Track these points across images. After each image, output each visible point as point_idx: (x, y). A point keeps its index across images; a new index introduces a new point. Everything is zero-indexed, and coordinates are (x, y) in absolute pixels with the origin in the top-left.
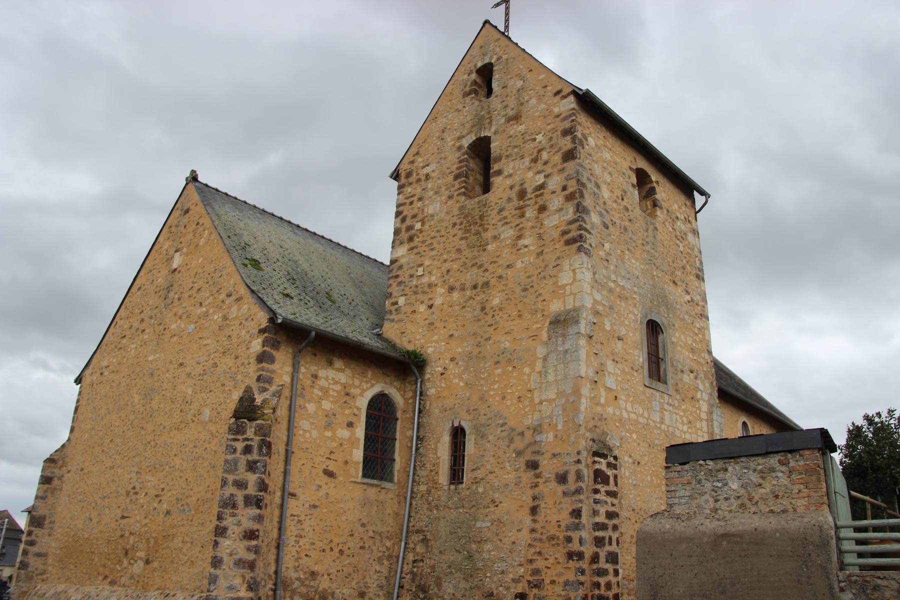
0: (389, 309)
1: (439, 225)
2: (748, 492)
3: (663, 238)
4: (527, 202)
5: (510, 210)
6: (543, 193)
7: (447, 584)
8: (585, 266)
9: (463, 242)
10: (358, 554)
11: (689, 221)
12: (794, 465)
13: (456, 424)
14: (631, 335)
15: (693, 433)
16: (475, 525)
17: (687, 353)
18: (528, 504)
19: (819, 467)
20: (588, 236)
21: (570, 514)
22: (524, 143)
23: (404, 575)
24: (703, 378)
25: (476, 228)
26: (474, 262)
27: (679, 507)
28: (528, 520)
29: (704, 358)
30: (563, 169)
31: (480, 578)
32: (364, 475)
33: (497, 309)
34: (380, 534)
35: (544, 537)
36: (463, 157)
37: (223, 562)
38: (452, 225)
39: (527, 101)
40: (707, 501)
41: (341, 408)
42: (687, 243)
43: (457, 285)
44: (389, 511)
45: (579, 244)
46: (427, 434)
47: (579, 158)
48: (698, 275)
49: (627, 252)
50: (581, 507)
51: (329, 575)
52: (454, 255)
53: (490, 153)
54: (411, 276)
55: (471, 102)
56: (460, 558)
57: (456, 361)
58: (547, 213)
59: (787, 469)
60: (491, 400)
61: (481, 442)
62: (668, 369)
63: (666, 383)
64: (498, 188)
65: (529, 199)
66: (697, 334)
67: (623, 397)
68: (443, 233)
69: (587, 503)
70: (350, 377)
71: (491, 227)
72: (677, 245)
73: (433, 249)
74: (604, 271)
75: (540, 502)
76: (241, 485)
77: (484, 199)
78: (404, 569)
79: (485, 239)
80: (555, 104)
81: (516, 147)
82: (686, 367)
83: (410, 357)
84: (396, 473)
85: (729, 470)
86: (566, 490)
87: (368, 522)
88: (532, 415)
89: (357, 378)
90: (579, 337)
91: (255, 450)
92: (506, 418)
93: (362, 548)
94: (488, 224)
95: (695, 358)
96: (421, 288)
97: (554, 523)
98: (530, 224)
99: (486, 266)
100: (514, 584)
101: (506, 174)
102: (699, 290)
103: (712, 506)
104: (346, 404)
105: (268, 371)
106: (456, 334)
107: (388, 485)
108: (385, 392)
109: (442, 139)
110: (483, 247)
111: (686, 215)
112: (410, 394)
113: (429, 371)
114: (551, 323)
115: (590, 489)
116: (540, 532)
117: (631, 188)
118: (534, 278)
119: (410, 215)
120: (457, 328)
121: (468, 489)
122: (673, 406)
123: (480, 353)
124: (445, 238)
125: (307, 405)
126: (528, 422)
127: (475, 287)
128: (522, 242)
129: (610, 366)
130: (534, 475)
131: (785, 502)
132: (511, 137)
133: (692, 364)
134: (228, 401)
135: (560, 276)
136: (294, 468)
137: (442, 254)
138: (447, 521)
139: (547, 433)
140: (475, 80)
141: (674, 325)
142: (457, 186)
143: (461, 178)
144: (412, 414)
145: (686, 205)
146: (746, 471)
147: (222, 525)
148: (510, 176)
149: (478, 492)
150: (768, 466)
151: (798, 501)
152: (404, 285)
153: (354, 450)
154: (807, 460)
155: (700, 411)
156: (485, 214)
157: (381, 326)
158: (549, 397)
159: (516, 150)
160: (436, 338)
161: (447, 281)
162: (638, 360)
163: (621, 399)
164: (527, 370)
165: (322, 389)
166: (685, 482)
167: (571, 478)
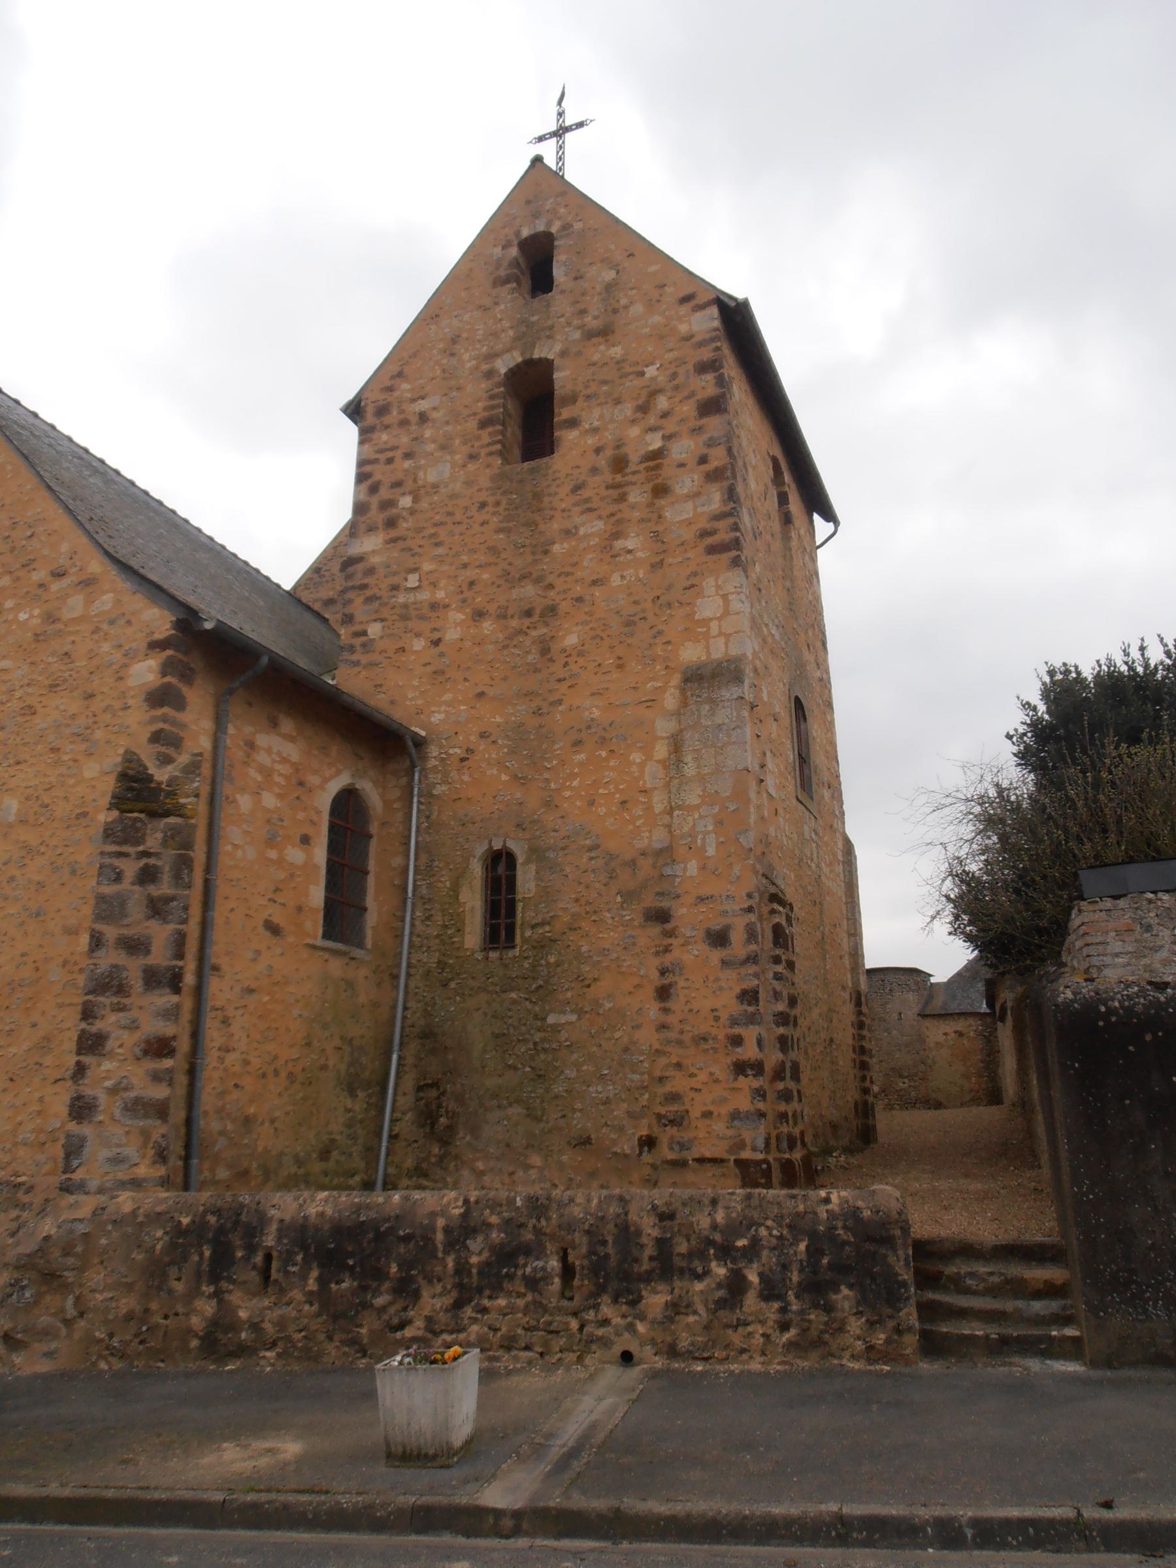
4: (630, 478)
5: (595, 487)
13: (497, 845)
22: (621, 377)
28: (653, 1011)
35: (687, 1038)
37: (96, 1106)
39: (626, 307)
43: (492, 608)
51: (272, 1121)
60: (565, 805)
65: (634, 473)
73: (437, 545)
75: (676, 978)
76: (135, 946)
78: (398, 1104)
81: (605, 382)
84: (369, 933)
88: (650, 832)
91: (166, 877)
96: (416, 609)
98: (637, 514)
101: (587, 426)
105: (174, 723)
106: (491, 692)
107: (358, 953)
112: (396, 793)
120: (492, 683)
125: (238, 796)
128: (619, 544)
134: (72, 782)
136: (219, 914)
137: (457, 555)
147: (94, 1029)
148: (595, 430)
160: (448, 697)
164: (636, 757)
165: (261, 769)
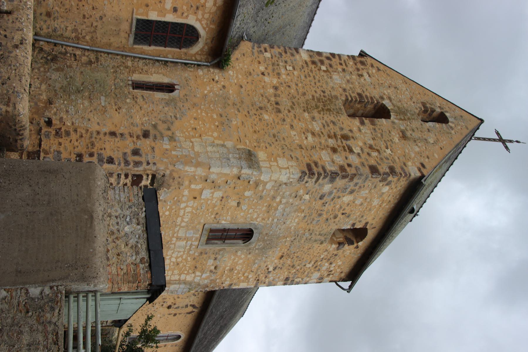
0: (262, 46)
1: (324, 81)
2: (122, 237)
3: (315, 248)
4: (339, 141)
6: (346, 151)
7: (58, 75)
8: (292, 176)
9: (311, 97)
10: (79, 13)
11: (329, 275)
12: (140, 267)
13: (176, 87)
14: (242, 214)
15: (170, 266)
16: (102, 95)
17: (229, 265)
18: (118, 130)
19: (139, 283)
20: (314, 180)
21: (110, 156)
23: (64, 47)
24: (212, 278)
25: (321, 106)
26: (296, 104)
27: (113, 194)
29: (225, 280)
30: (364, 165)
31: (63, 97)
32: (138, 20)
33: (261, 117)
34: (95, 32)
35: (93, 139)
36: (375, 100)
38: (324, 90)
39: (417, 145)
40: (116, 211)
41: (187, 3)
42: (312, 271)
43: (279, 92)
44: (112, 40)
45: (308, 172)
46: (169, 68)
47: (372, 177)
48: (288, 280)
49: (303, 215)
50: (115, 164)
52: (301, 91)
53: (378, 118)
54: (286, 62)
55: (417, 107)
56: (78, 84)
57: (223, 89)
58: (331, 153)
59: (138, 262)
61: (163, 103)
62: (217, 246)
63: (207, 244)
64: (351, 122)
66: (244, 274)
67: (196, 204)
68: (318, 84)
69: (118, 169)
70: (210, 10)
71: (321, 116)
72: (311, 262)
73: (306, 77)
74: (288, 193)
77: (342, 113)
78: (69, 48)
79: (313, 111)
80: (414, 163)
81: (382, 135)
82: (219, 263)
83: (225, 55)
84: (140, 47)
85: (138, 226)
86: (127, 154)
87: (103, 22)
88: (183, 137)
89: (209, 16)
90: (239, 168)
92: (181, 119)
93: (84, 16)
94: (324, 114)
95: (226, 272)
96: (277, 68)
97: (103, 146)
98: (323, 141)
99: (292, 111)
100: (58, 118)
102: (277, 280)
103: (113, 214)
104: (190, 6)
106: (243, 90)
108: (200, 39)
109: (389, 87)
110: (306, 110)
111: (333, 272)
112: (198, 58)
113: (215, 71)
114: (249, 151)
115: (128, 171)
116: (97, 137)
117: (351, 222)
118: (283, 142)
119: (332, 63)
120: (247, 91)
121: (129, 92)
122: (190, 250)
123: (229, 105)
124: (314, 85)
126: (178, 133)
127: (277, 103)
129: (218, 194)
130: (139, 135)
131: (115, 260)
132: (390, 132)
133: (221, 269)
135: (284, 159)
137: (301, 83)
138: (105, 78)
139: (170, 145)
140: (435, 111)
141: (250, 253)
142: (353, 95)
143: (359, 98)
144: (184, 59)
145: (342, 272)
146: (137, 237)
148: (360, 130)
149: (126, 99)
150: (140, 251)
151: (115, 268)
152: (280, 57)
153: (156, 13)
154: (144, 275)
155: (186, 274)
156: (331, 112)
157: (250, 40)
158: (195, 147)
159: (379, 135)
160: (240, 76)
161: (281, 85)
162: (224, 220)
163: (194, 203)
164: (215, 134)
166: (130, 198)
167: (137, 158)
